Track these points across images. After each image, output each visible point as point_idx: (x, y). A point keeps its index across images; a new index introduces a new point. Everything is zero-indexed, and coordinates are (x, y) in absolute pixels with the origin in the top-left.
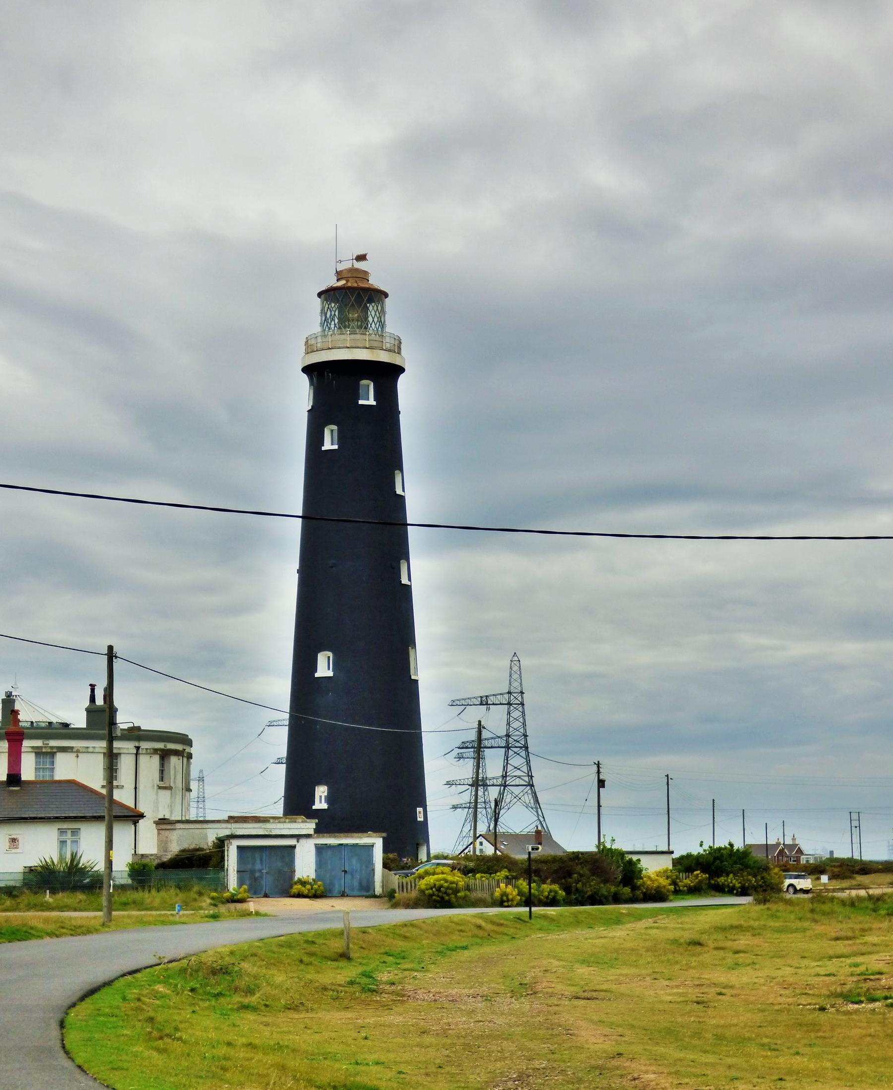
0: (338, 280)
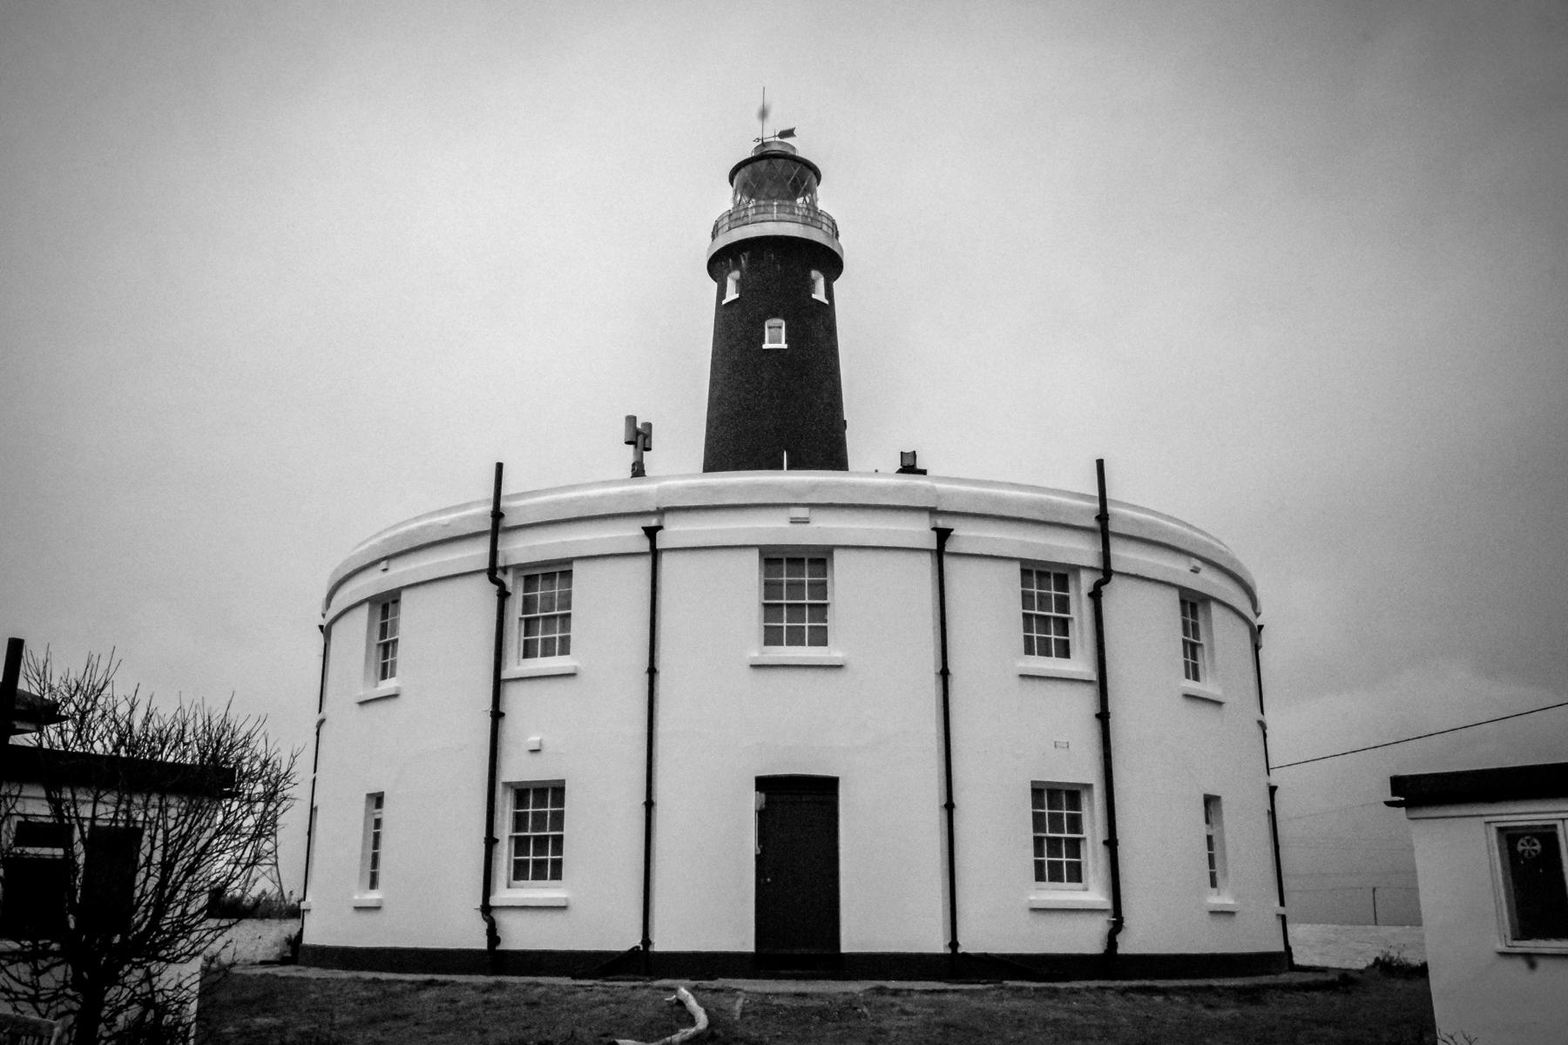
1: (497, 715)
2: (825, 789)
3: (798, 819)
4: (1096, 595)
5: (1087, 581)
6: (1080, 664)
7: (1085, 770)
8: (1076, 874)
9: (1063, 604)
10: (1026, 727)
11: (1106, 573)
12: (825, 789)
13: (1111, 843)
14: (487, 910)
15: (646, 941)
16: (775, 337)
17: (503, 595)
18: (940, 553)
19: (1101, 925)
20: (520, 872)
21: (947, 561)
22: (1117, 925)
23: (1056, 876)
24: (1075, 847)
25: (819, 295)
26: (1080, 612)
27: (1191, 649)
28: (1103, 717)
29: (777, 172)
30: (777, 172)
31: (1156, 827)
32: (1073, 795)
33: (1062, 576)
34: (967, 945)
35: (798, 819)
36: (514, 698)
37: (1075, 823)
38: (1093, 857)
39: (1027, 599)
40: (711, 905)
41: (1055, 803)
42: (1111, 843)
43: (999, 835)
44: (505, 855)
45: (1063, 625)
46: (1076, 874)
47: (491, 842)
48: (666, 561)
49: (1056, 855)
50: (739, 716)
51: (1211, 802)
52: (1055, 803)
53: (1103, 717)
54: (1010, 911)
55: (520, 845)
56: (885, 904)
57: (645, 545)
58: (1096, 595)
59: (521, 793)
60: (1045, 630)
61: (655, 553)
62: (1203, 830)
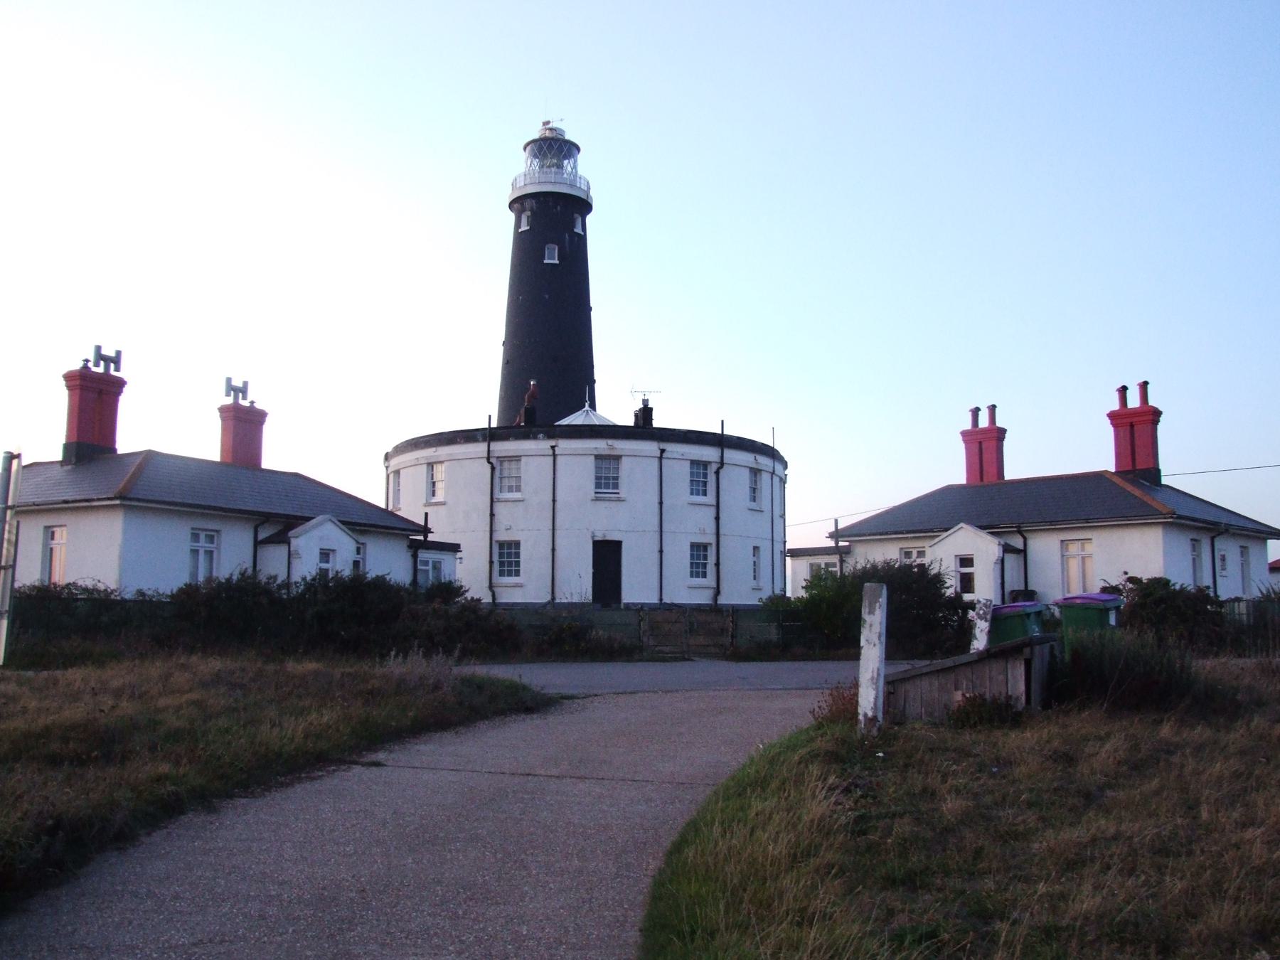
0: (618, 458)
1: (492, 515)
2: (617, 545)
3: (607, 556)
4: (717, 473)
5: (714, 467)
6: (710, 499)
7: (711, 539)
8: (704, 575)
9: (705, 476)
10: (691, 522)
11: (722, 464)
12: (617, 545)
13: (717, 564)
14: (491, 587)
15: (553, 598)
16: (552, 258)
17: (493, 469)
18: (661, 458)
19: (710, 593)
20: (502, 574)
21: (664, 461)
22: (717, 592)
23: (698, 576)
24: (705, 565)
25: (578, 230)
26: (711, 479)
27: (754, 490)
28: (717, 518)
29: (553, 148)
30: (553, 148)
31: (736, 559)
32: (705, 547)
33: (705, 465)
34: (667, 600)
35: (607, 556)
36: (499, 508)
37: (705, 557)
38: (711, 569)
39: (692, 474)
40: (578, 585)
41: (699, 550)
42: (717, 564)
43: (679, 557)
44: (496, 567)
45: (705, 484)
46: (704, 575)
47: (491, 562)
48: (559, 459)
49: (698, 568)
50: (588, 520)
51: (756, 549)
52: (699, 550)
53: (717, 518)
54: (686, 591)
55: (502, 564)
56: (637, 587)
57: (551, 452)
58: (717, 473)
59: (501, 545)
60: (698, 486)
61: (554, 455)
62: (752, 559)
